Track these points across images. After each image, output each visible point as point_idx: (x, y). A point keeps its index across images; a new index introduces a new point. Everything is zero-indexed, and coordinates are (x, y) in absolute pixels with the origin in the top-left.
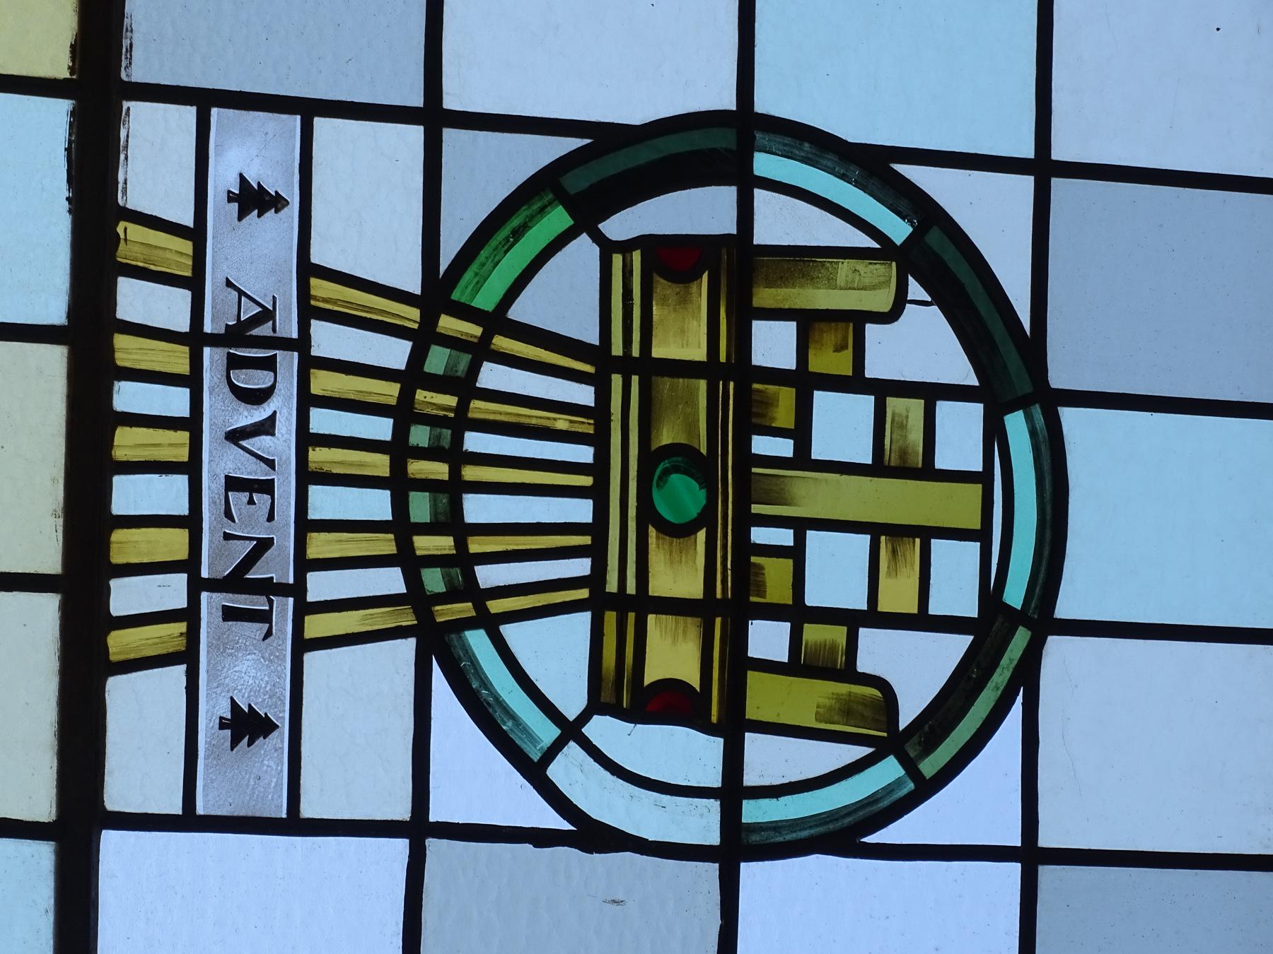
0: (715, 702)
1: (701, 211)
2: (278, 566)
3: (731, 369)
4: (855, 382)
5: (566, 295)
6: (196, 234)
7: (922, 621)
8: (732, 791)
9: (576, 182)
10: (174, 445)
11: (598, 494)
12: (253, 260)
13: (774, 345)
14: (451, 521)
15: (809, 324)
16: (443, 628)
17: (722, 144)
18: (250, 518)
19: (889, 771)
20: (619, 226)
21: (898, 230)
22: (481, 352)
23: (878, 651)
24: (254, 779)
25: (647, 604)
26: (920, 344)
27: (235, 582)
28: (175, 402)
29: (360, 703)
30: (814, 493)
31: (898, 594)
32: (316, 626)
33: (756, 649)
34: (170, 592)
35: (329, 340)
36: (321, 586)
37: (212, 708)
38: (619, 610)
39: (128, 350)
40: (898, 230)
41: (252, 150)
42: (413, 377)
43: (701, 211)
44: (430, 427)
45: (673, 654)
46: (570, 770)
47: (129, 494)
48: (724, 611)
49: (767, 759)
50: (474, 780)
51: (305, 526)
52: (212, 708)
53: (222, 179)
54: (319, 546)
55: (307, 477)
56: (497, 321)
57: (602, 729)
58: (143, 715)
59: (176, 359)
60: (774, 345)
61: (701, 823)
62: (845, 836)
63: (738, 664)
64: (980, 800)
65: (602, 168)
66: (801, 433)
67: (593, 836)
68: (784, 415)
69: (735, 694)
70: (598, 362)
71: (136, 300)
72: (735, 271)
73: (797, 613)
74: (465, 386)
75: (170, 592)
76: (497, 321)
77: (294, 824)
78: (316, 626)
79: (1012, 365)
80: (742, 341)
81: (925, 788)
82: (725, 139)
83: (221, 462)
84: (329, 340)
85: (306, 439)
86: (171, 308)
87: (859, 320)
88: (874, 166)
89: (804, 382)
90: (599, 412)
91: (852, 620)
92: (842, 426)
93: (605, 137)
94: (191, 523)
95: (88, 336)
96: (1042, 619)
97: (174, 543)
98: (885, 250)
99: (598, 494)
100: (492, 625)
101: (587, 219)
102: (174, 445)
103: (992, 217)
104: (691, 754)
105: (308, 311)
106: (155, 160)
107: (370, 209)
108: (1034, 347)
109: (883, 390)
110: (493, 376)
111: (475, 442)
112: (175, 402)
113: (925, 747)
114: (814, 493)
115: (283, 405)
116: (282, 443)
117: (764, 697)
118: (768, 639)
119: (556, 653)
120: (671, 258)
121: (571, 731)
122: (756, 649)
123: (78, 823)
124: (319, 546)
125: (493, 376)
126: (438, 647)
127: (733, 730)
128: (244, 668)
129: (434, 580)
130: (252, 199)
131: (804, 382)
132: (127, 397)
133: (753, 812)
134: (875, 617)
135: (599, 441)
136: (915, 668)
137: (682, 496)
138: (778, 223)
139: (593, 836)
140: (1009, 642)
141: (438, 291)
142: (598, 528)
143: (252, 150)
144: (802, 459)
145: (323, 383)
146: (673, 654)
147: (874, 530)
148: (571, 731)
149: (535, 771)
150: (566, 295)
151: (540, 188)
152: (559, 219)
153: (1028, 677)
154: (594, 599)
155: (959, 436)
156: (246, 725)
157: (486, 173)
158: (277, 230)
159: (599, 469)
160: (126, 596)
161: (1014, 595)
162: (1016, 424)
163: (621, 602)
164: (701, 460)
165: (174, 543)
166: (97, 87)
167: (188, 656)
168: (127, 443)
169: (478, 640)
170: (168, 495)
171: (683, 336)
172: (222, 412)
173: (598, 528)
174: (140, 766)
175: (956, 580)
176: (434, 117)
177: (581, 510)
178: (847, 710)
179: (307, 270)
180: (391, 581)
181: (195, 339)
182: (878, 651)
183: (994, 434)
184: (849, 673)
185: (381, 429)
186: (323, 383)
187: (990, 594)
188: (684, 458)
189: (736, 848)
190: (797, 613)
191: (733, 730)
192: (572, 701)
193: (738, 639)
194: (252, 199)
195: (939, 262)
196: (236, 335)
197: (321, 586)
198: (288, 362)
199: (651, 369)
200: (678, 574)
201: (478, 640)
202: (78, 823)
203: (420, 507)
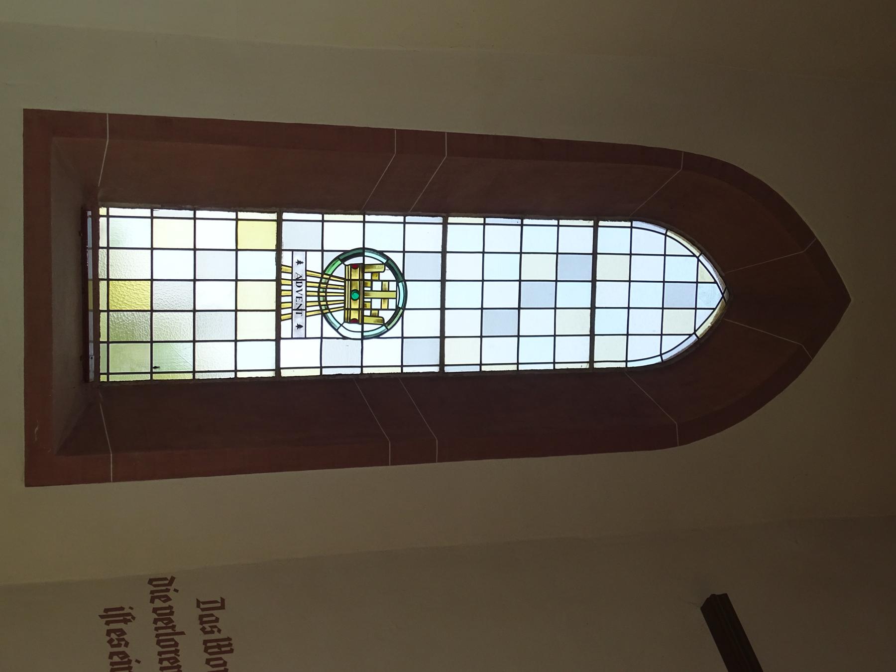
0: (361, 321)
1: (358, 260)
2: (303, 307)
3: (363, 280)
4: (379, 280)
5: (340, 271)
6: (292, 267)
7: (388, 309)
8: (362, 332)
9: (341, 258)
10: (290, 293)
11: (345, 296)
12: (299, 270)
13: (368, 276)
14: (326, 301)
15: (372, 273)
16: (324, 313)
17: (361, 252)
18: (299, 301)
19: (384, 328)
20: (346, 263)
21: (384, 261)
22: (329, 279)
23: (381, 313)
24: (301, 333)
25: (351, 309)
26: (388, 275)
27: (297, 309)
28: (290, 288)
29: (314, 324)
30: (373, 295)
31: (384, 307)
32: (308, 314)
33: (101, 213)
34: (289, 311)
35: (309, 279)
36: (308, 309)
37: (295, 325)
38: (348, 310)
39: (283, 282)
40: (384, 261)
41: (299, 256)
42: (320, 283)
43: (358, 260)
44: (323, 289)
45: (355, 315)
46: (341, 330)
47: (283, 299)
48: (362, 309)
49: (367, 327)
50: (329, 331)
51: (306, 302)
52: (295, 325)
53: (295, 260)
54: (308, 304)
55: (306, 296)
56: (331, 275)
57: (345, 325)
58: (286, 326)
59: (290, 283)
60: (368, 276)
61: (359, 336)
62: (378, 336)
63: (363, 316)
64: (396, 331)
65: (345, 256)
66: (371, 287)
67: (344, 338)
68: (369, 285)
69: (363, 320)
70: (345, 280)
71: (284, 276)
72: (363, 267)
73: (371, 309)
74: (327, 284)
75: (289, 311)
76: (331, 275)
77: (306, 338)
78: (308, 314)
79: (400, 277)
80: (363, 276)
81: (388, 330)
82: (361, 251)
83: (295, 295)
84: (309, 279)
85: (306, 291)
86: (289, 276)
87: (379, 272)
88: (381, 253)
89: (372, 281)
90: (345, 286)
91: (378, 310)
92: (377, 286)
93: (345, 252)
94: (292, 302)
95: (278, 280)
96: (404, 308)
97: (290, 305)
98: (383, 263)
99: (345, 296)
100: (331, 313)
101: (343, 261)
102: (290, 293)
103: (397, 259)
104: (358, 327)
105: (306, 276)
106: (286, 258)
107: (315, 263)
108: (403, 275)
109: (382, 281)
110: (330, 282)
111: (328, 290)
112: (290, 288)
113: (388, 325)
114: (373, 295)
115: (303, 287)
116: (303, 292)
117: (366, 320)
118: (367, 313)
119: (340, 316)
120: (354, 266)
121: (341, 325)
122: (101, 213)
123: (278, 339)
124: (308, 304)
125: (330, 282)
126: (324, 315)
127: (363, 324)
128: (299, 319)
129: (323, 308)
130: (299, 262)
131: (372, 281)
132: (283, 288)
133: (365, 334)
134: (381, 309)
135: (345, 289)
136: (387, 315)
137: (356, 296)
138: (368, 261)
139: (344, 338)
140: (399, 312)
141: (323, 272)
142: (345, 300)
143: (299, 256)
144: (372, 290)
145: (308, 284)
146: (355, 315)
147: (389, 291)
148: (341, 325)
149: (337, 330)
150: (340, 271)
151: (337, 258)
152: (339, 262)
153: (402, 315)
154: (345, 309)
155: (393, 286)
156: (299, 326)
157: (329, 257)
158: (302, 266)
159: (345, 293)
160: (283, 312)
161: (400, 306)
162: (400, 284)
163: (348, 309)
164: (359, 291)
165: (290, 305)
166: (279, 250)
167: (292, 318)
168: (283, 293)
169: (329, 315)
170: (289, 299)
171: (356, 275)
172: (295, 289)
173: (345, 300)
174: (286, 331)
175: (392, 304)
176: (323, 251)
177: (343, 298)
178: (378, 321)
179: (306, 271)
180: (318, 308)
181: (292, 280)
182: (381, 313)
183: (397, 285)
184: (378, 316)
185: (316, 289)
186: (308, 284)
187: (397, 306)
188: (356, 291)
189: (363, 338)
190: (371, 309)
191: (363, 324)
192: (341, 322)
193: (363, 313)
194: (299, 262)
195: (390, 265)
196: (297, 279)
197: (308, 309)
198: (304, 282)
199: (351, 280)
200: (355, 305)
201: (329, 315)
202: (278, 339)
203: (321, 299)
